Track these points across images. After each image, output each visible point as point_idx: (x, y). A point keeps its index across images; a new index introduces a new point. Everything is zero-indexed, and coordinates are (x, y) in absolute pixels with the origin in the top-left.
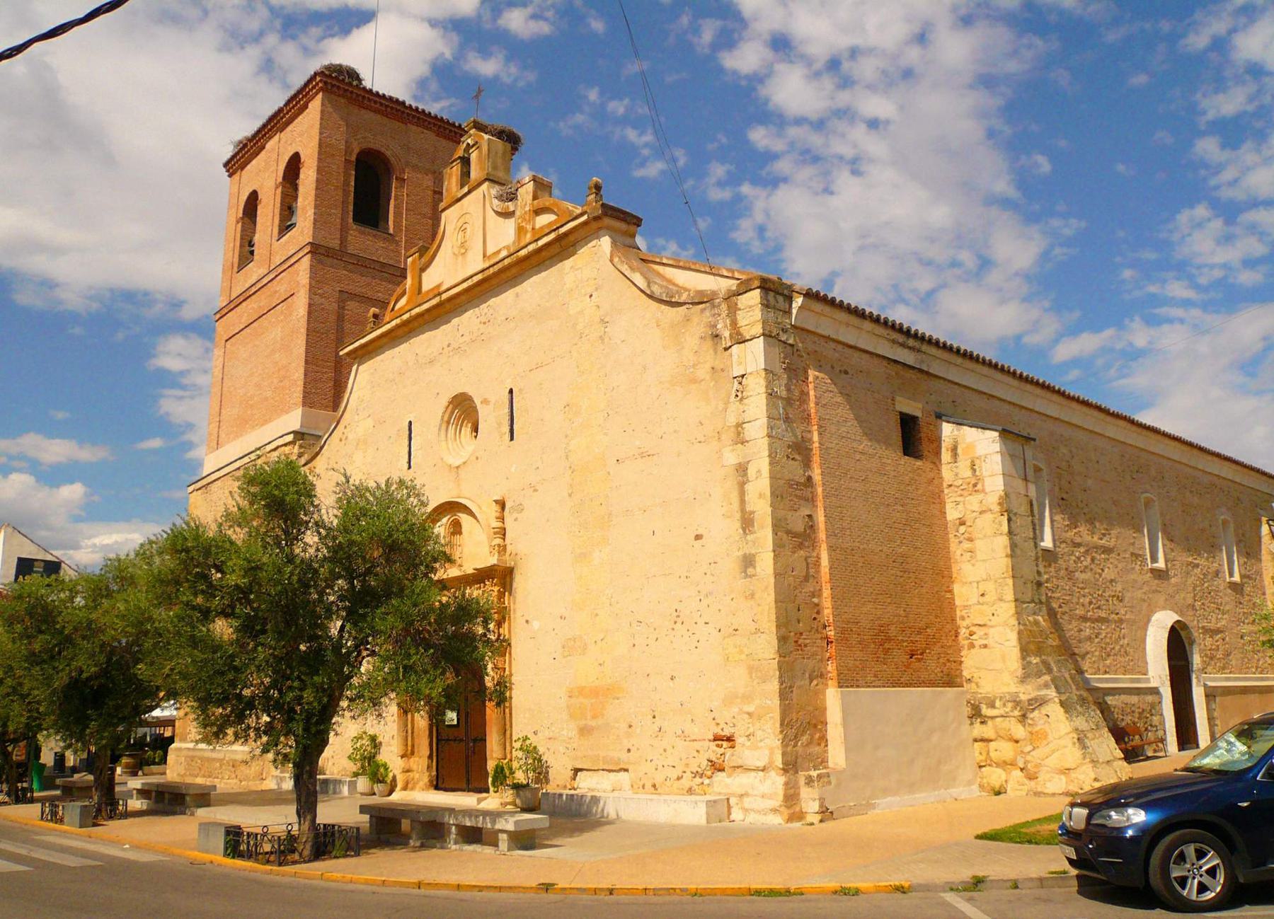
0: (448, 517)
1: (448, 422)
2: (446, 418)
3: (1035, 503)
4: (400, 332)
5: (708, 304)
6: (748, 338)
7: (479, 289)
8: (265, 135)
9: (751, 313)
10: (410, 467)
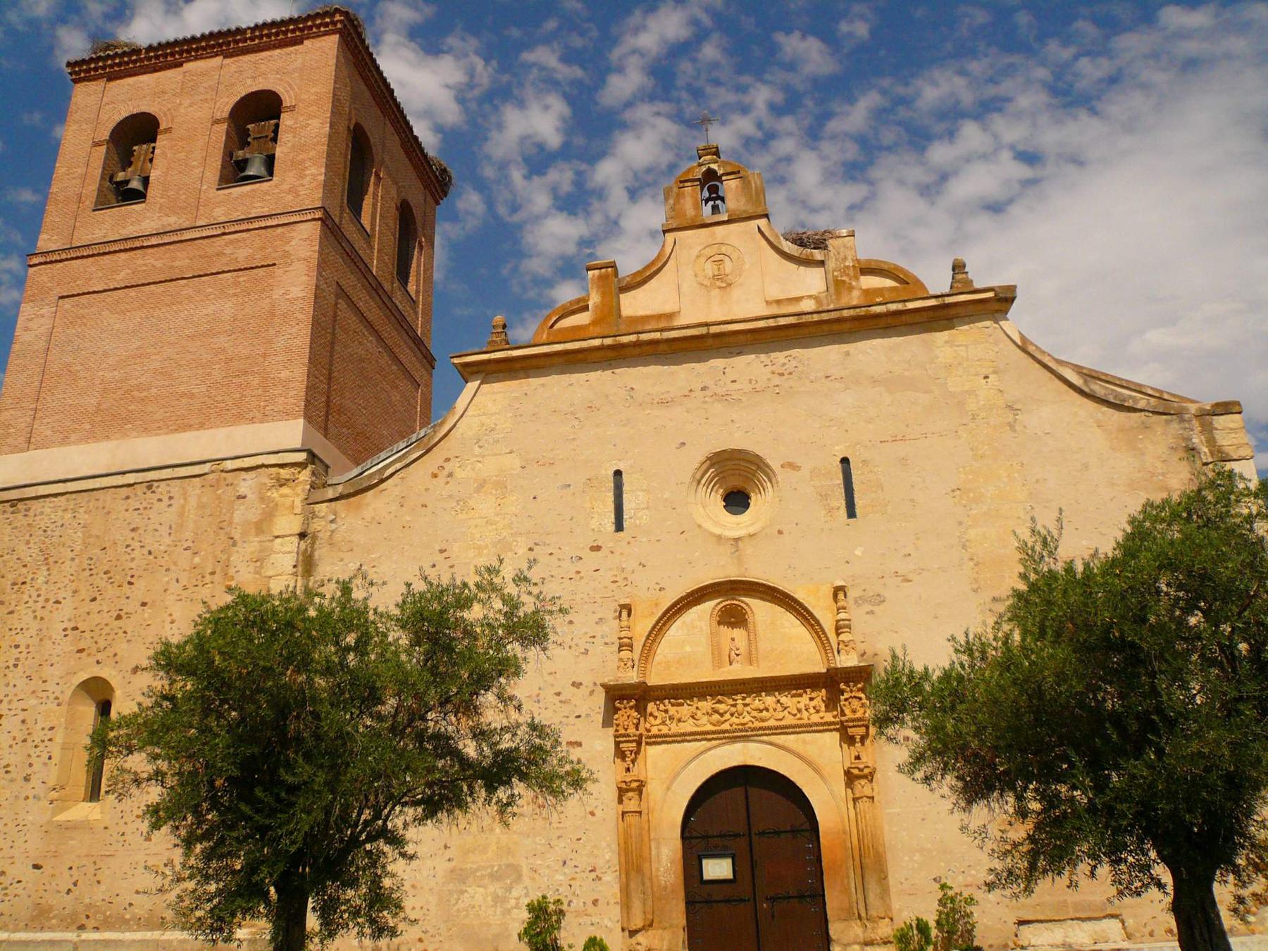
0: (719, 600)
1: (699, 482)
2: (698, 476)
3: (836, 653)
4: (600, 354)
5: (1175, 417)
6: (1235, 457)
7: (931, 314)
8: (213, 46)
9: (1233, 435)
10: (619, 526)
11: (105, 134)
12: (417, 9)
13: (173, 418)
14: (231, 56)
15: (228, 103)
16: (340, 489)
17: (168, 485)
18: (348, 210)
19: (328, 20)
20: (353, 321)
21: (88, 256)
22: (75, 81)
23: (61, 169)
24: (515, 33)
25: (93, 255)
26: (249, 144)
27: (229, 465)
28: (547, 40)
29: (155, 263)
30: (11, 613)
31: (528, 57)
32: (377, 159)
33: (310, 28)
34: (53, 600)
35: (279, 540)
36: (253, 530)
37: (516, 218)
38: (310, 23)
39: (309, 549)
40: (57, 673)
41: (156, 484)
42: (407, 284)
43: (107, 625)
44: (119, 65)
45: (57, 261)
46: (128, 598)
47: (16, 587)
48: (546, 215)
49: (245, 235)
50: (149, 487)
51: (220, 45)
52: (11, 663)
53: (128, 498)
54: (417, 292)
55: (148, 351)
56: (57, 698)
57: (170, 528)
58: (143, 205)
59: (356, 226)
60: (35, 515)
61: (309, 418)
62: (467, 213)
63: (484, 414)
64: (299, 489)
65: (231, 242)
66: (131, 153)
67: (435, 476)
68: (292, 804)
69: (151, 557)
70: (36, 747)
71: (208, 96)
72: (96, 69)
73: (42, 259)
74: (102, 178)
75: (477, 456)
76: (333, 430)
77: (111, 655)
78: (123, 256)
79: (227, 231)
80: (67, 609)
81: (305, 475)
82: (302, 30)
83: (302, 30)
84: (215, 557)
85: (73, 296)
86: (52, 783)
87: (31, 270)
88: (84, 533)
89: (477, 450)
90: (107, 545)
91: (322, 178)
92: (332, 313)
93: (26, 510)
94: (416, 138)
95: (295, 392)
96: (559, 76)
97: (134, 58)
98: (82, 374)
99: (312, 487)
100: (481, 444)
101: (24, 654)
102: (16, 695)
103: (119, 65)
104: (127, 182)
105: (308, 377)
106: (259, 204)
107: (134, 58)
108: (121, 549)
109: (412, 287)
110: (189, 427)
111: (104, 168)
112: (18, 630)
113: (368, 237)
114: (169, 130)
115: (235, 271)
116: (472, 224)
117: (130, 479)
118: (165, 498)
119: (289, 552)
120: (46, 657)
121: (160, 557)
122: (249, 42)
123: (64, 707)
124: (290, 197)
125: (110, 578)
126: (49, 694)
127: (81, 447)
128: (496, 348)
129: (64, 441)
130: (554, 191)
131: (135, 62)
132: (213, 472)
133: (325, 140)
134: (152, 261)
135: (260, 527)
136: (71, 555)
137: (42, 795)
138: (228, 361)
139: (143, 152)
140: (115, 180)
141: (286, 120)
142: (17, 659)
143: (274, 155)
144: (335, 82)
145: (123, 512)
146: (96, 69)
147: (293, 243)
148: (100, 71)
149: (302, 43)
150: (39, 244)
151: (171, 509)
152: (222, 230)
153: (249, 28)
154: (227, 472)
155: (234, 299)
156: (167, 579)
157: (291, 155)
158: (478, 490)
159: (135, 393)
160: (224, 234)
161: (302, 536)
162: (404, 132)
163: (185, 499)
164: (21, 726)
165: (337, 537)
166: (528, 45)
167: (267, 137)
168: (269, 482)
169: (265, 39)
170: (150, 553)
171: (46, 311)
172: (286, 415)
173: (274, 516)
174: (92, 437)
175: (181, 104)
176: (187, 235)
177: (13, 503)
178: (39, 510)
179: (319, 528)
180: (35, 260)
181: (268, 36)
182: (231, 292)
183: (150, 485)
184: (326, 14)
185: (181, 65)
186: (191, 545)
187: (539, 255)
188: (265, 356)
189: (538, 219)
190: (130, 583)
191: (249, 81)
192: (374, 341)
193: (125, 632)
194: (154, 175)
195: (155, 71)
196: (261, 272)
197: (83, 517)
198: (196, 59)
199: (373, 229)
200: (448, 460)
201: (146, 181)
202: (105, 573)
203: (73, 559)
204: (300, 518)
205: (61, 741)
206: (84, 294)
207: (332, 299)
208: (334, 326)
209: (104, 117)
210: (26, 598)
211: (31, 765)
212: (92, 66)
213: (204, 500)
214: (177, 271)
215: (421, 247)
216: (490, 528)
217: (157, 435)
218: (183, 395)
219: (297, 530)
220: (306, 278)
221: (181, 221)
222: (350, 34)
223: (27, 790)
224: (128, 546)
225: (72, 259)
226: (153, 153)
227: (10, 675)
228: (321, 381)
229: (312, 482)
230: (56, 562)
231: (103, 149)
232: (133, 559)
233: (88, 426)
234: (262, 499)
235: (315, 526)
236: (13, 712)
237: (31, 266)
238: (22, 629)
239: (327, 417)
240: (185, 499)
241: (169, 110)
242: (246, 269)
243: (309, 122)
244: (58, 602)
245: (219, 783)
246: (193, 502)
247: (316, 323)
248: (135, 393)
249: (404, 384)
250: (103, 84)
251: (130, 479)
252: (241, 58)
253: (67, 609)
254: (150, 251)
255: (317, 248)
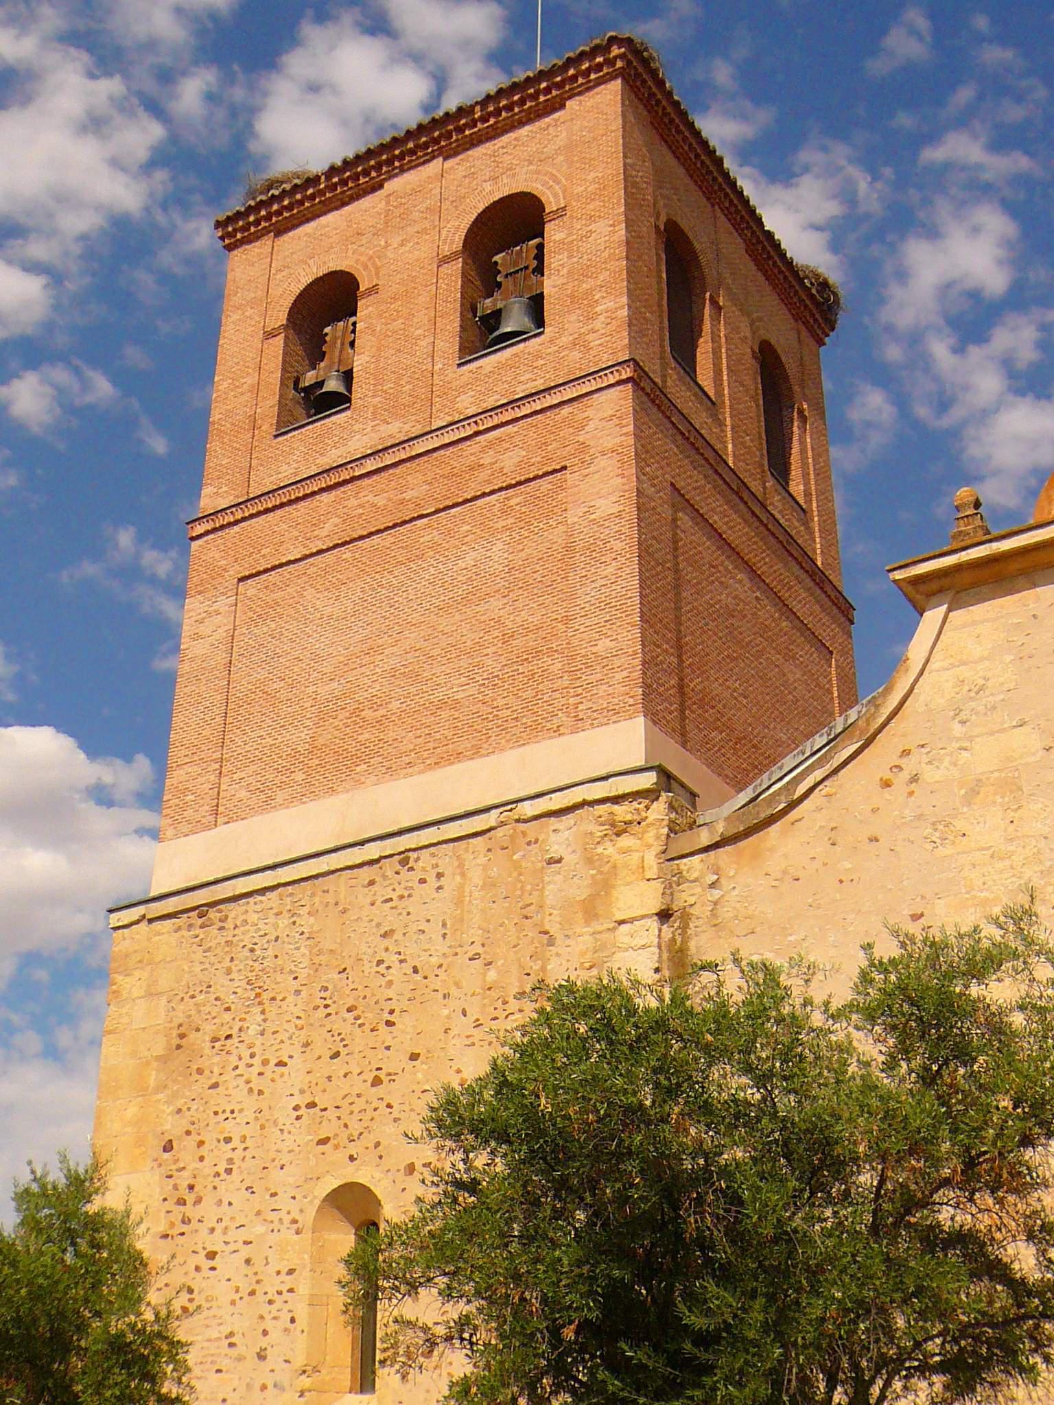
8: (426, 146)
11: (280, 317)
12: (744, 117)
13: (431, 745)
14: (456, 154)
15: (458, 228)
16: (720, 828)
17: (433, 855)
18: (673, 364)
19: (600, 59)
20: (707, 549)
21: (275, 508)
22: (229, 248)
23: (221, 382)
24: (904, 120)
25: (282, 505)
26: (499, 285)
27: (529, 809)
28: (962, 122)
29: (376, 500)
30: (215, 1086)
31: (934, 154)
32: (710, 273)
33: (574, 78)
34: (273, 1061)
35: (624, 928)
36: (580, 915)
37: (945, 422)
38: (571, 72)
39: (679, 939)
40: (291, 1180)
41: (413, 855)
42: (787, 483)
43: (359, 1096)
44: (289, 208)
45: (230, 525)
46: (388, 1048)
47: (217, 1045)
48: (998, 407)
49: (509, 429)
50: (404, 862)
51: (436, 141)
52: (221, 1168)
53: (372, 883)
54: (807, 494)
55: (380, 642)
56: (295, 1221)
57: (444, 925)
58: (348, 413)
59: (689, 389)
60: (236, 927)
61: (653, 716)
62: (869, 425)
63: (964, 663)
64: (650, 836)
65: (490, 445)
66: (322, 339)
67: (887, 784)
68: (709, 1369)
69: (418, 977)
70: (270, 1302)
71: (427, 224)
72: (257, 222)
73: (209, 526)
74: (283, 384)
75: (958, 739)
76: (693, 735)
77: (371, 1145)
78: (326, 498)
79: (481, 428)
80: (295, 1076)
81: (658, 810)
82: (560, 86)
83: (560, 86)
84: (521, 967)
85: (259, 573)
86: (299, 1361)
87: (195, 545)
88: (310, 948)
89: (957, 729)
90: (347, 963)
91: (625, 312)
92: (669, 535)
93: (221, 921)
94: (769, 235)
95: (625, 674)
96: (988, 176)
97: (310, 191)
98: (283, 695)
99: (671, 830)
100: (963, 716)
101: (239, 1152)
102: (232, 1218)
103: (289, 208)
104: (320, 384)
105: (643, 645)
106: (528, 376)
107: (310, 191)
108: (370, 968)
109: (797, 488)
110: (459, 756)
111: (284, 370)
112: (228, 1114)
113: (713, 405)
114: (373, 290)
115: (501, 489)
116: (876, 440)
117: (373, 851)
118: (431, 879)
119: (644, 947)
120: (272, 1155)
121: (432, 977)
122: (479, 125)
123: (307, 1236)
124: (576, 355)
125: (357, 1018)
126: (283, 1214)
127: (293, 811)
128: (969, 542)
129: (268, 805)
130: (1007, 364)
131: (313, 197)
132: (503, 824)
133: (622, 252)
134: (370, 497)
135: (590, 909)
136: (295, 985)
137: (286, 1384)
138: (506, 639)
139: (339, 334)
140: (302, 385)
141: (554, 233)
142: (230, 1161)
143: (542, 293)
144: (625, 156)
145: (368, 907)
146: (257, 222)
147: (591, 426)
148: (263, 224)
149: (563, 106)
150: (202, 504)
151: (442, 893)
152: (475, 428)
153: (477, 103)
154: (525, 821)
155: (505, 536)
156: (446, 1012)
157: (570, 286)
158: (968, 800)
159: (368, 713)
160: (477, 434)
161: (664, 916)
162: (749, 228)
163: (463, 875)
164: (245, 1270)
165: (726, 912)
166: (932, 137)
167: (526, 268)
168: (598, 831)
169: (504, 114)
170: (416, 971)
171: (223, 604)
172: (612, 714)
173: (613, 887)
174: (306, 793)
175: (387, 245)
176: (419, 448)
177: (201, 910)
178: (242, 918)
179: (692, 900)
180: (199, 529)
181: (509, 108)
182: (499, 525)
183: (404, 858)
184: (596, 50)
185: (380, 186)
186: (480, 950)
187: (996, 473)
188: (567, 620)
189: (984, 416)
190: (389, 1024)
191: (488, 187)
192: (746, 581)
193: (389, 1106)
194: (360, 363)
195: (344, 204)
196: (544, 484)
197: (307, 922)
198: (403, 170)
199: (719, 392)
200: (906, 753)
201: (348, 377)
202: (349, 1010)
203: (298, 992)
204: (658, 886)
205: (307, 1292)
206: (274, 568)
207: (667, 512)
208: (676, 557)
209: (275, 292)
210: (233, 1060)
211: (265, 1333)
212: (252, 219)
213: (494, 872)
214: (411, 506)
215: (803, 419)
216: (1000, 865)
217: (407, 776)
218: (441, 706)
219: (655, 906)
220: (620, 480)
221: (407, 427)
222: (638, 75)
223: (262, 1374)
224: (380, 962)
225: (252, 516)
226: (354, 331)
227: (222, 1187)
228: (666, 651)
229: (671, 821)
230: (273, 999)
231: (280, 340)
232: (390, 983)
233: (299, 776)
234: (590, 861)
235: (684, 896)
236: (232, 1247)
237: (193, 539)
238: (232, 1112)
239: (682, 712)
240: (463, 875)
241: (371, 258)
242: (519, 483)
243: (593, 227)
244: (281, 1064)
245: (569, 1333)
246: (476, 876)
247: (645, 553)
248: (368, 713)
249: (805, 652)
250: (269, 243)
251: (373, 851)
252: (470, 153)
253: (295, 1076)
254: (366, 482)
255: (631, 428)
